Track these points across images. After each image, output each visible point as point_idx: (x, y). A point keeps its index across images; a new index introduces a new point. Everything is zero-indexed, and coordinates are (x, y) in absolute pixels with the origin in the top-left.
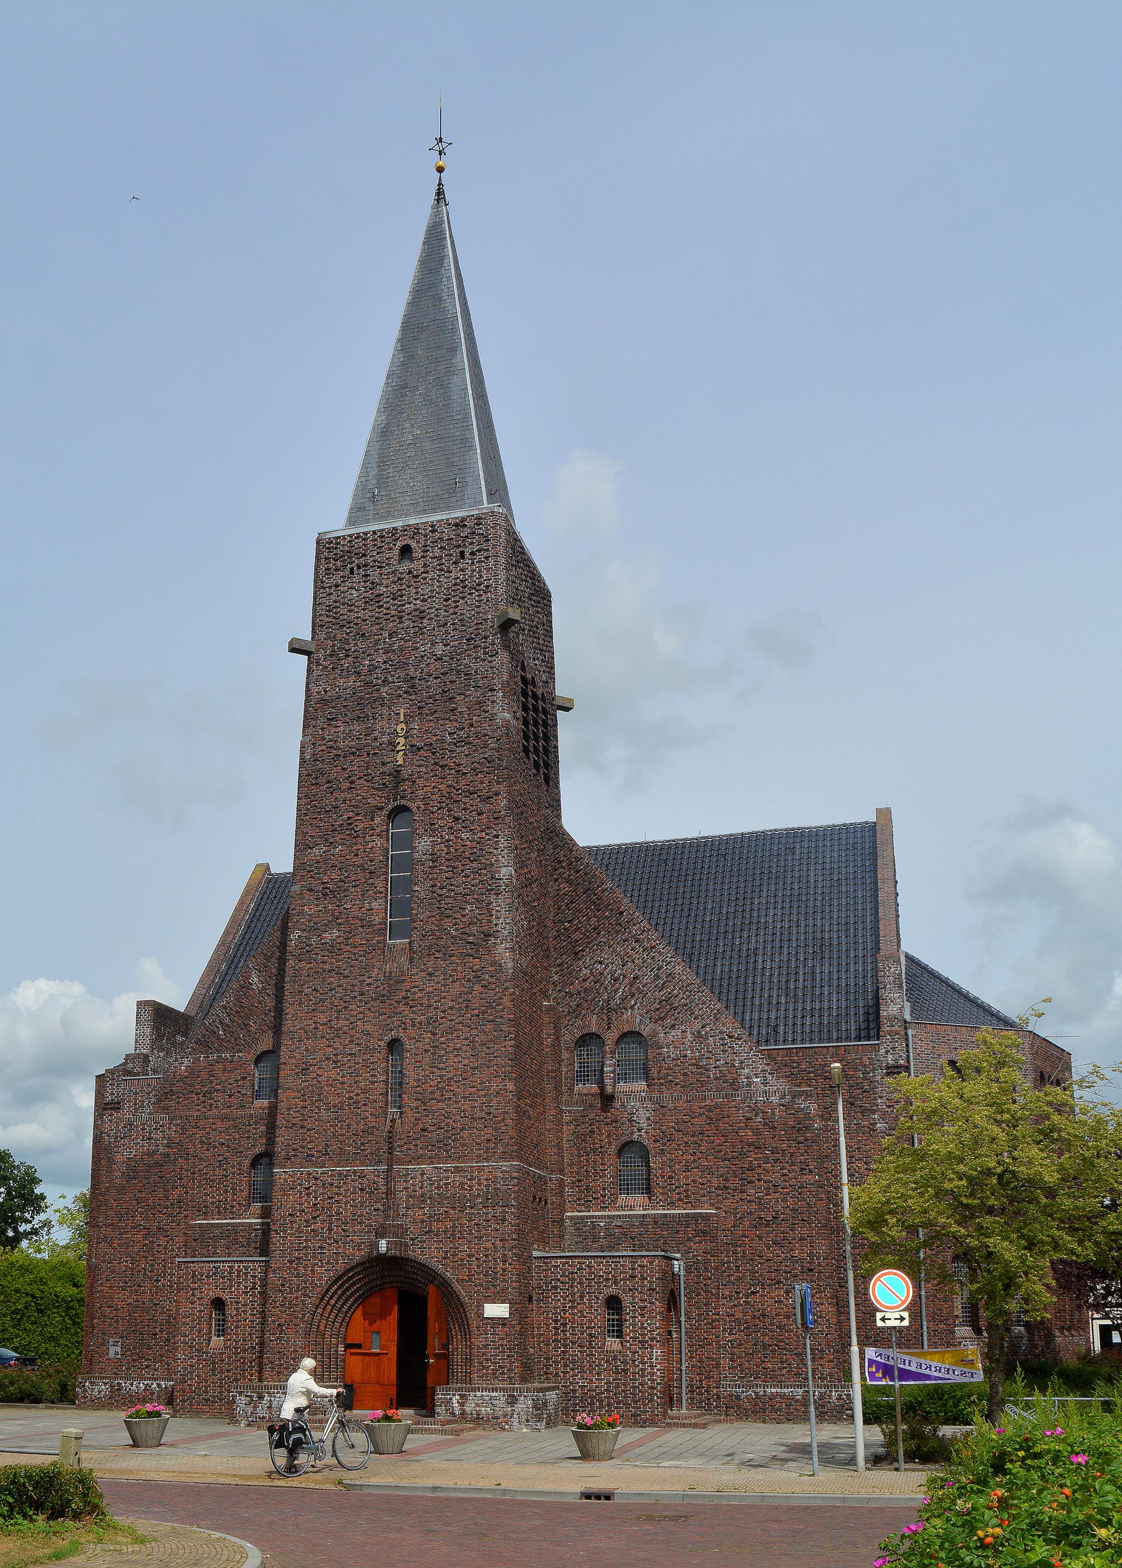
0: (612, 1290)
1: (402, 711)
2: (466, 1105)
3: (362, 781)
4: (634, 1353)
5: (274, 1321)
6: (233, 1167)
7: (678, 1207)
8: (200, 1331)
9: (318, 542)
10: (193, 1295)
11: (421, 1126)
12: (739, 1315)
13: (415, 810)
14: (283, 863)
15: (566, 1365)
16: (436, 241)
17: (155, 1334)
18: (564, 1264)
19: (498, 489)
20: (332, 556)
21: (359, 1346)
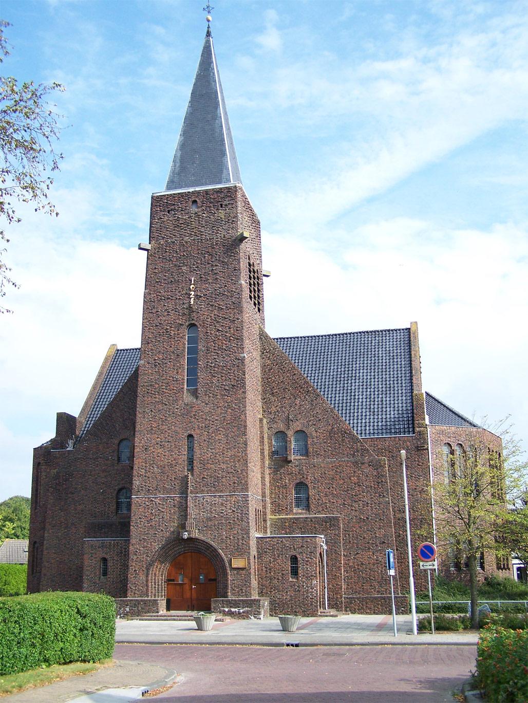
0: (293, 553)
1: (193, 279)
2: (224, 466)
3: (173, 312)
4: (303, 582)
5: (132, 569)
6: (109, 494)
7: (322, 514)
8: (95, 573)
9: (152, 197)
10: (91, 556)
11: (202, 476)
12: (351, 564)
13: (199, 326)
14: (132, 339)
15: (271, 588)
16: (207, 52)
17: (71, 575)
18: (270, 541)
19: (238, 178)
20: (157, 202)
21: (173, 580)
